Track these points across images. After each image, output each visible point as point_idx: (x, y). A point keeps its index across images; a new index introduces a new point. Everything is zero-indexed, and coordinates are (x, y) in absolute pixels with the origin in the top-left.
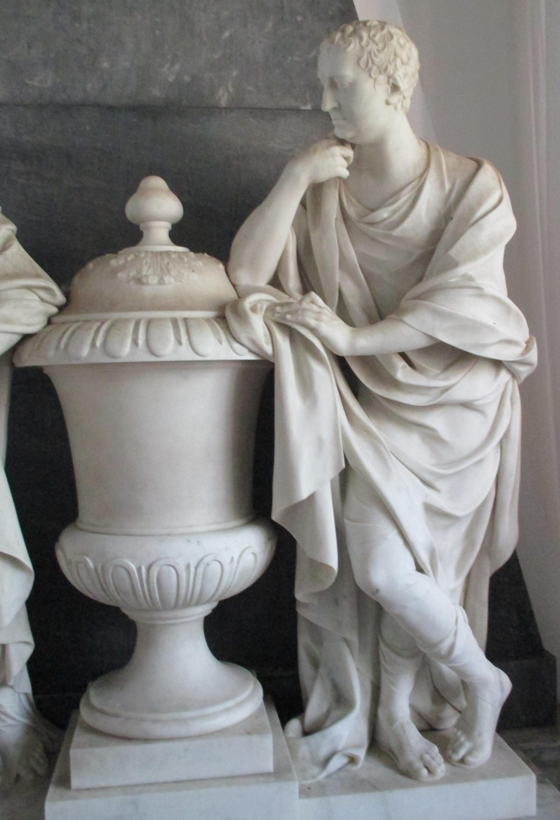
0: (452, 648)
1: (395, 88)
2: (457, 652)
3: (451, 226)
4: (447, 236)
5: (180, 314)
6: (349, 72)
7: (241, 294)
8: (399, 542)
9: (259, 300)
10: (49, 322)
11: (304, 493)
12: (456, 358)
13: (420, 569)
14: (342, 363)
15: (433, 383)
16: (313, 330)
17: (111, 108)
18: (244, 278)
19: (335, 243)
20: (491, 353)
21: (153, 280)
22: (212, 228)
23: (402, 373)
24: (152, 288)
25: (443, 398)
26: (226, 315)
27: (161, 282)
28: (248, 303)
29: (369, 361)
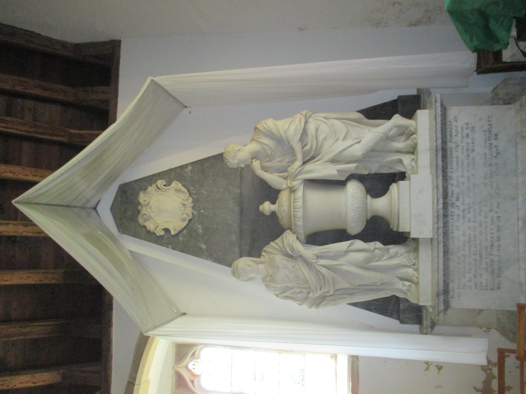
0: (382, 133)
1: (239, 150)
6: (236, 161)
8: (351, 148)
9: (289, 183)
10: (294, 233)
11: (336, 172)
13: (359, 142)
14: (304, 163)
15: (311, 139)
16: (296, 170)
17: (241, 220)
18: (284, 186)
19: (275, 163)
23: (307, 148)
26: (292, 190)
28: (290, 185)
29: (304, 155)
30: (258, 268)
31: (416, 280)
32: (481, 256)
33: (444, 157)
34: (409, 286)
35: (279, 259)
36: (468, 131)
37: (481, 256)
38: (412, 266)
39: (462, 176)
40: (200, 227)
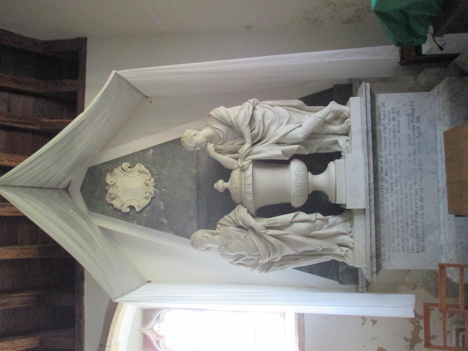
1: (195, 135)
2: (322, 117)
3: (224, 121)
4: (226, 123)
5: (243, 179)
6: (192, 145)
7: (239, 167)
8: (293, 131)
10: (245, 207)
12: (252, 118)
13: (301, 126)
16: (246, 152)
19: (228, 146)
20: (251, 112)
21: (236, 185)
22: (225, 173)
23: (255, 131)
24: (238, 185)
25: (261, 121)
26: (243, 170)
27: (236, 183)
28: (240, 165)
29: (253, 139)
30: (214, 239)
31: (352, 245)
32: (407, 223)
33: (374, 137)
34: (346, 251)
35: (232, 229)
36: (394, 115)
37: (407, 223)
38: (349, 234)
39: (390, 154)
40: (162, 203)
